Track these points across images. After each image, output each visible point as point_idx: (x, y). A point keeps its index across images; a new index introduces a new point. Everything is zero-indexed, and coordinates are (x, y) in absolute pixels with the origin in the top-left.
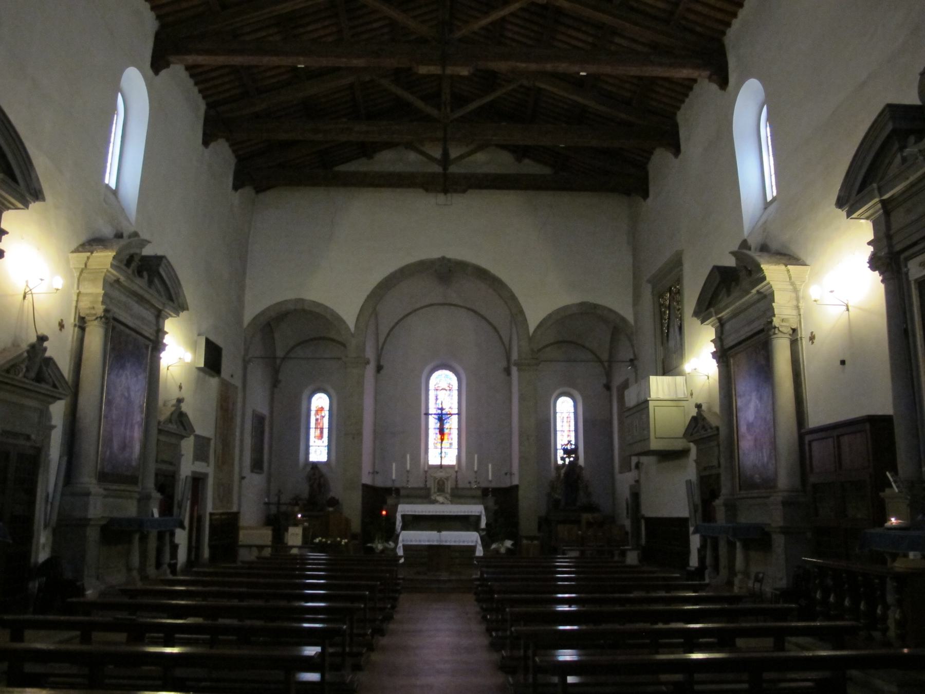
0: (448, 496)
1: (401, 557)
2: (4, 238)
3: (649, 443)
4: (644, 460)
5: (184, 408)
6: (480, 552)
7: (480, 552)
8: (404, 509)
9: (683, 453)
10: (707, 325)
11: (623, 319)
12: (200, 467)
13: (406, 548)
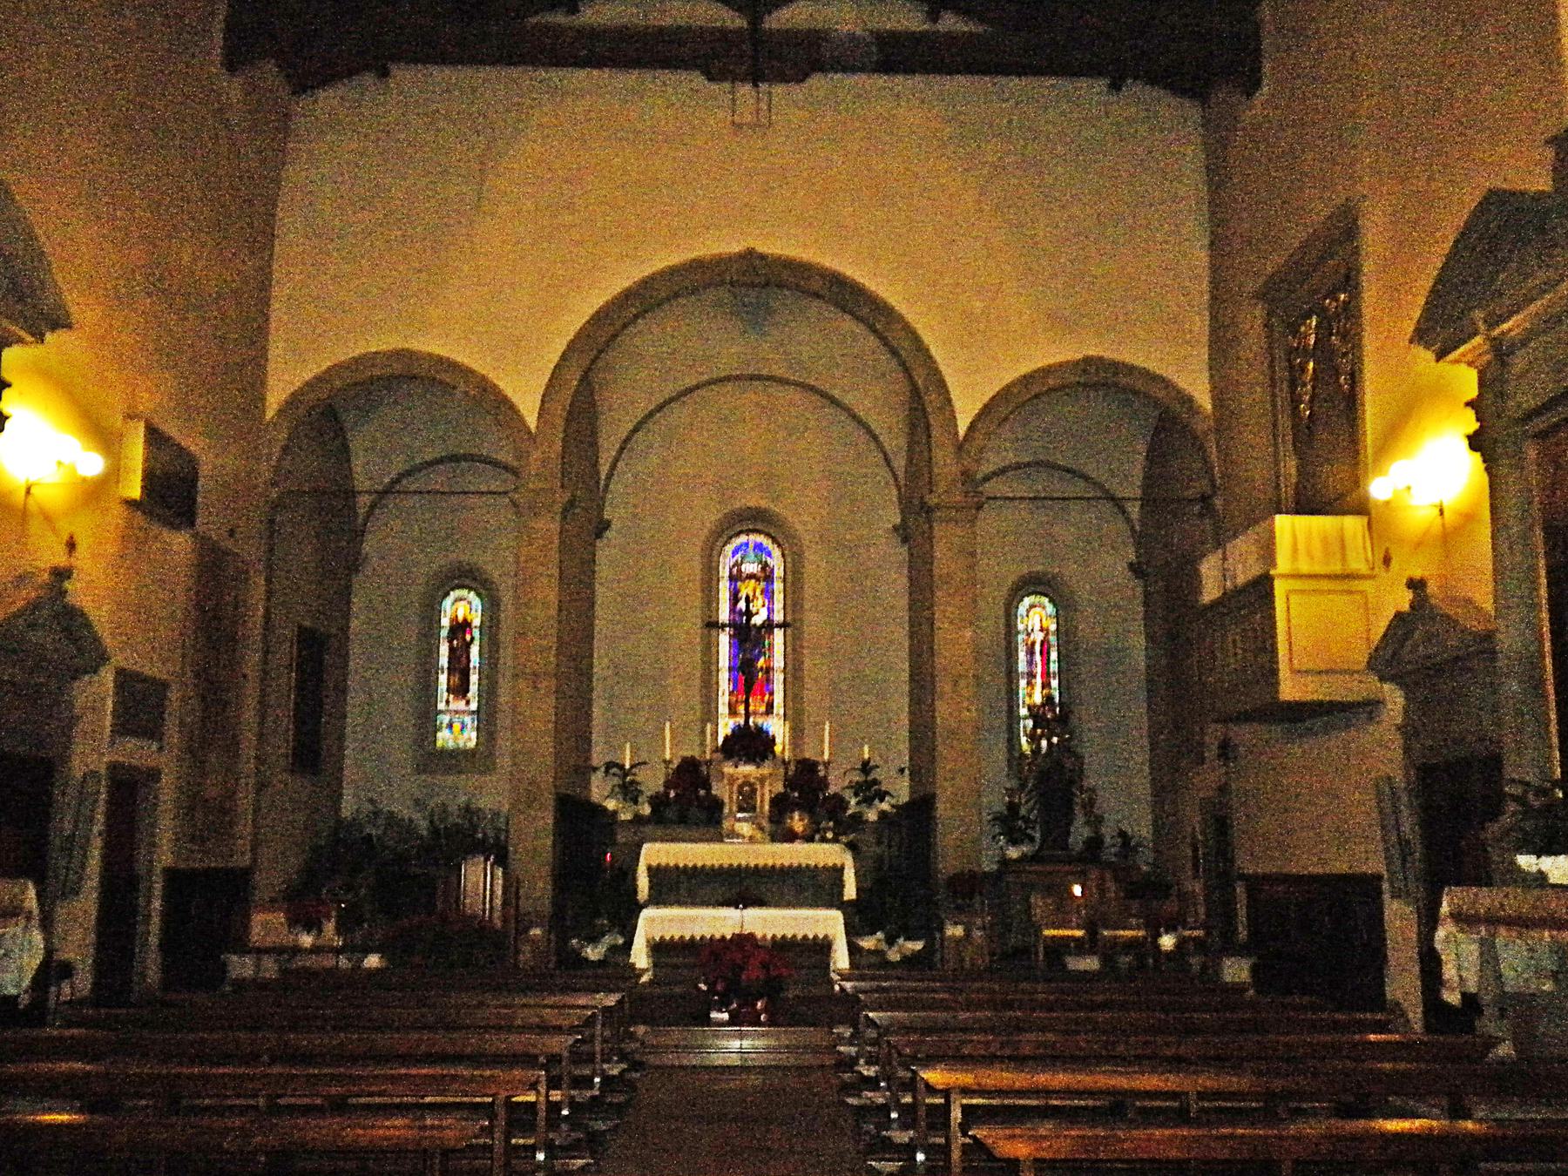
0: (765, 823)
1: (644, 971)
2: (6, 393)
3: (1276, 684)
4: (1244, 734)
5: (78, 593)
6: (841, 959)
7: (841, 959)
8: (655, 853)
9: (1370, 708)
10: (1457, 361)
11: (1188, 401)
12: (136, 752)
13: (659, 949)
